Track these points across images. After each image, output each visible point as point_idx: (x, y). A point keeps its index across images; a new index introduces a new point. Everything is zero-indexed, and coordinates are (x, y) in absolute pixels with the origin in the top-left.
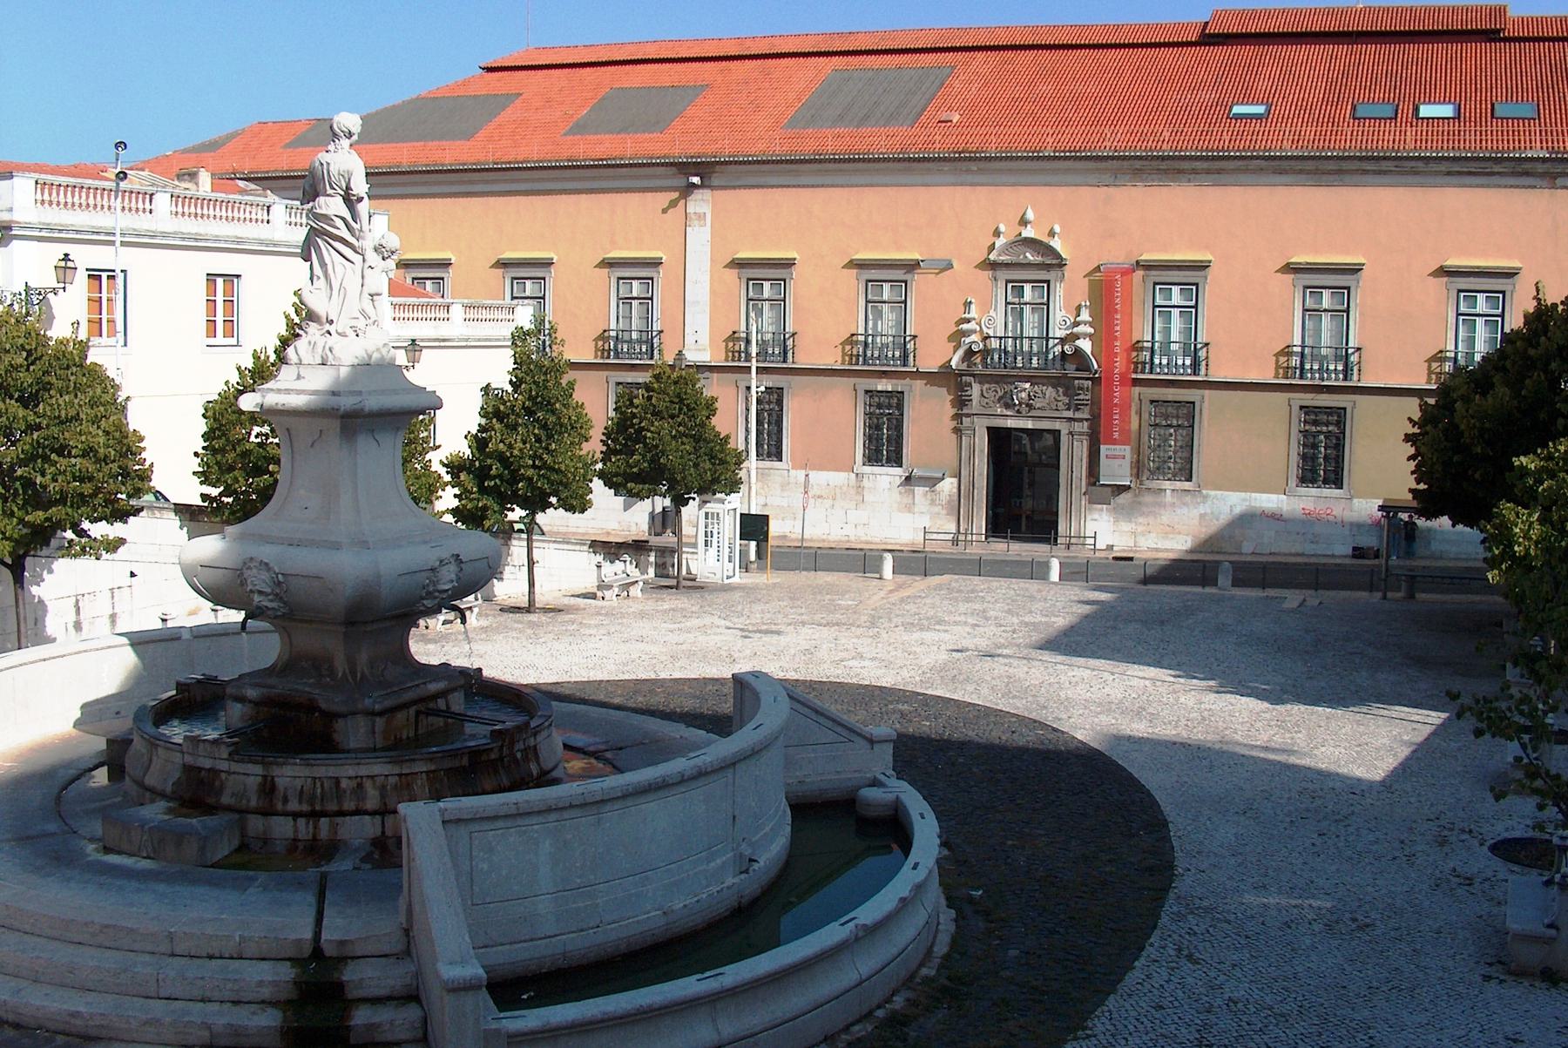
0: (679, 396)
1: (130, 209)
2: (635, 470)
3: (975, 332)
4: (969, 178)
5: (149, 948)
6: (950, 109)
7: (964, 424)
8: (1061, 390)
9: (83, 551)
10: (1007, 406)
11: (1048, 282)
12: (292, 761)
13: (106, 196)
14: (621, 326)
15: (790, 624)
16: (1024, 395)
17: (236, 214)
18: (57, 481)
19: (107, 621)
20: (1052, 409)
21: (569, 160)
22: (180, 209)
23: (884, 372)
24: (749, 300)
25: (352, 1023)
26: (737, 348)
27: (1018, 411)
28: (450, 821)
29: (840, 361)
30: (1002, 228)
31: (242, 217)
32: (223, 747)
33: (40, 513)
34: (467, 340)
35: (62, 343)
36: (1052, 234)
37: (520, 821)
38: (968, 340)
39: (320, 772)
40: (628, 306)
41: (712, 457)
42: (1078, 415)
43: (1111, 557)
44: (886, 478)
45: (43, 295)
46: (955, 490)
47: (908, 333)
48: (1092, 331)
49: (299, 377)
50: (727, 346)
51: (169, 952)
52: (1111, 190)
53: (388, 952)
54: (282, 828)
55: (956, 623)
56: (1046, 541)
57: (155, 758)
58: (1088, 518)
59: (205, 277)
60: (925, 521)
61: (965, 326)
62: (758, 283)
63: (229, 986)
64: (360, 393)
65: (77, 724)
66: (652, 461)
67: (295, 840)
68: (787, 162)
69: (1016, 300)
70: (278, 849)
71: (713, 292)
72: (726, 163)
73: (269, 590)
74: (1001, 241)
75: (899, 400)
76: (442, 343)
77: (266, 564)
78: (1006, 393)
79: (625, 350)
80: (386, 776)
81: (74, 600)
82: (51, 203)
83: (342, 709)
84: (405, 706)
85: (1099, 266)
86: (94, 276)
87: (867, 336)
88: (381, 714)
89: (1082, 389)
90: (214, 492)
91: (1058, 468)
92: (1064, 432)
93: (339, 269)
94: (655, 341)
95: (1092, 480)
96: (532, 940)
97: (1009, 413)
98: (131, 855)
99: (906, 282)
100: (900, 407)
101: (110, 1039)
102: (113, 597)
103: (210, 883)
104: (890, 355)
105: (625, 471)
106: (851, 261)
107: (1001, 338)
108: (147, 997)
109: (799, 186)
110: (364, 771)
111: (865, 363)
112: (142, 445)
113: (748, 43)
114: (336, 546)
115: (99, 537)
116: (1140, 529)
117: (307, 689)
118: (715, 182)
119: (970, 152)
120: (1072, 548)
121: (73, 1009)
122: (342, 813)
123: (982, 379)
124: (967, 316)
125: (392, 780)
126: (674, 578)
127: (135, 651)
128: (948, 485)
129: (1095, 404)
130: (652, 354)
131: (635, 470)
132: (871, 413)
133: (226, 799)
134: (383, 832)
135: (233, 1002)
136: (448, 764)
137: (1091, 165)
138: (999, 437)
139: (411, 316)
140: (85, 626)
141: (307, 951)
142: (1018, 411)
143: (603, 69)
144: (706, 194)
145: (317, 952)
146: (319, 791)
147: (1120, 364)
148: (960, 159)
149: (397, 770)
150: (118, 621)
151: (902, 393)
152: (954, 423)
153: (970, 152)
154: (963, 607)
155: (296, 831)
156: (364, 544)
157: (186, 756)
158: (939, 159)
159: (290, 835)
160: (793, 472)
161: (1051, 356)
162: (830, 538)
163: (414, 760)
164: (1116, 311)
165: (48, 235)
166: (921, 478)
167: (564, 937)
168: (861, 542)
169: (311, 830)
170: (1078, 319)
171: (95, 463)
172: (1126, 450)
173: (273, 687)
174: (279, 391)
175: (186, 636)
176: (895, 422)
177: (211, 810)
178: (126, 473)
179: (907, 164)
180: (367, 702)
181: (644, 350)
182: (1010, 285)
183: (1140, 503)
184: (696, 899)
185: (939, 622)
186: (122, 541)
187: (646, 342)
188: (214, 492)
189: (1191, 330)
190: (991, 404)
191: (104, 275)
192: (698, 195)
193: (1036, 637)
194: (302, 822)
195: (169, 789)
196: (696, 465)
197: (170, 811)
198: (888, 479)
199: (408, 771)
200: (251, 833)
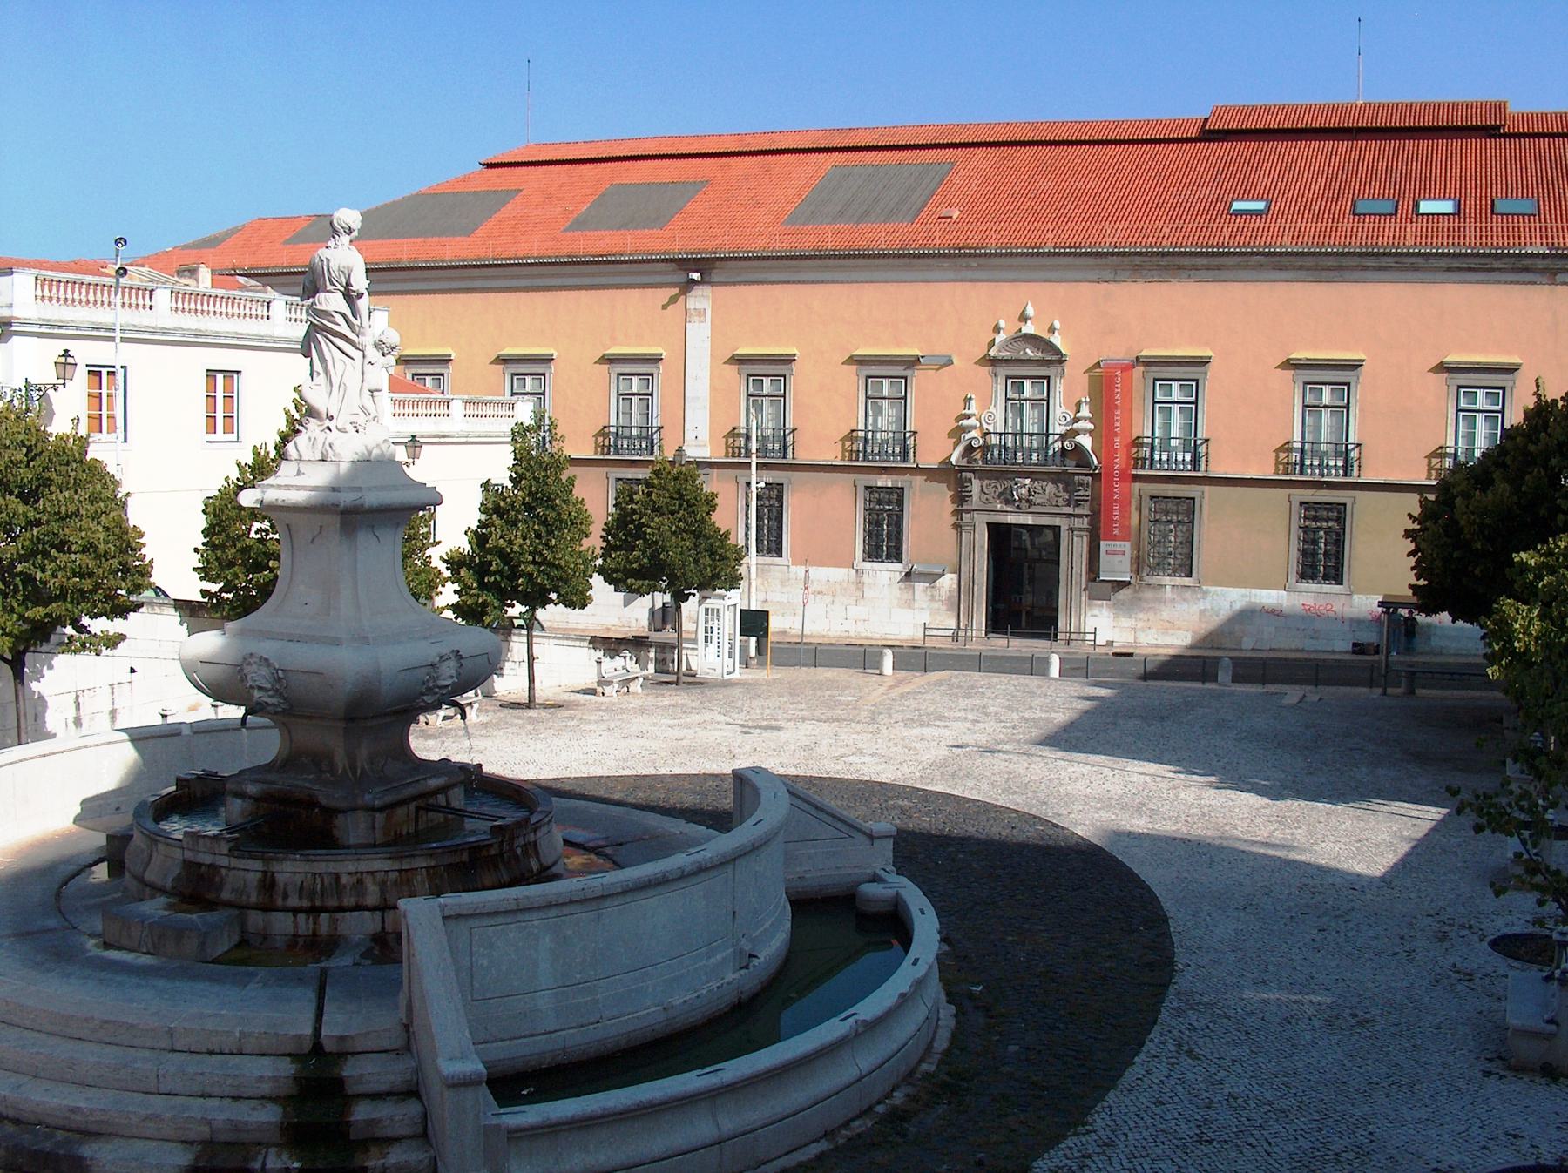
0: (679, 492)
1: (130, 305)
2: (635, 566)
3: (975, 428)
4: (969, 274)
6: (950, 205)
7: (964, 520)
8: (1061, 486)
9: (83, 647)
10: (1007, 502)
11: (1048, 378)
12: (292, 856)
13: (106, 292)
14: (621, 422)
15: (790, 720)
16: (1024, 491)
17: (236, 310)
19: (107, 717)
21: (569, 257)
22: (180, 305)
23: (884, 468)
24: (749, 396)
26: (737, 444)
27: (1018, 507)
28: (449, 917)
29: (840, 458)
30: (1002, 324)
31: (242, 313)
32: (223, 843)
36: (1052, 330)
37: (520, 917)
38: (968, 436)
39: (321, 867)
41: (712, 553)
42: (1078, 511)
44: (887, 573)
46: (955, 586)
47: (908, 429)
49: (299, 473)
50: (727, 442)
52: (1111, 286)
54: (282, 924)
55: (956, 719)
56: (1046, 637)
57: (155, 854)
58: (1088, 614)
60: (925, 617)
61: (965, 422)
62: (758, 379)
63: (229, 1081)
64: (360, 489)
65: (77, 820)
66: (652, 557)
67: (295, 936)
68: (787, 258)
69: (1016, 396)
70: (278, 945)
71: (713, 388)
72: (726, 259)
73: (269, 686)
74: (1000, 338)
75: (899, 496)
76: (442, 439)
77: (266, 660)
78: (1005, 489)
79: (625, 446)
81: (74, 695)
82: (51, 299)
83: (343, 805)
86: (94, 372)
87: (867, 432)
88: (381, 809)
89: (1082, 485)
90: (214, 588)
91: (1058, 564)
92: (1064, 528)
93: (339, 365)
94: (655, 436)
95: (1093, 576)
96: (532, 1035)
97: (1008, 509)
98: (131, 950)
99: (906, 378)
100: (900, 502)
102: (113, 693)
103: (213, 979)
105: (625, 566)
106: (851, 357)
107: (1001, 434)
108: (147, 1093)
109: (799, 282)
110: (363, 866)
111: (865, 459)
112: (142, 541)
114: (336, 642)
115: (99, 633)
118: (715, 278)
119: (970, 248)
120: (1072, 644)
121: (73, 1104)
122: (341, 909)
123: (982, 475)
124: (967, 411)
126: (674, 674)
127: (136, 747)
128: (948, 581)
129: (1095, 500)
130: (652, 450)
131: (635, 566)
132: (871, 509)
133: (226, 895)
134: (383, 928)
135: (233, 1098)
137: (1091, 261)
138: (999, 534)
139: (411, 412)
140: (85, 722)
141: (307, 1046)
142: (1018, 507)
145: (317, 1048)
146: (319, 886)
147: (1120, 461)
148: (960, 255)
149: (397, 866)
151: (902, 488)
152: (954, 520)
153: (970, 248)
154: (963, 703)
155: (296, 927)
156: (364, 640)
158: (940, 255)
159: (290, 930)
160: (793, 568)
161: (1051, 452)
162: (830, 634)
163: (413, 856)
165: (48, 331)
166: (920, 574)
167: (564, 1032)
168: (862, 638)
169: (311, 926)
170: (1078, 415)
171: (95, 559)
173: (273, 783)
174: (279, 487)
175: (186, 732)
176: (895, 518)
177: (211, 905)
178: (126, 569)
179: (907, 261)
181: (644, 446)
182: (1010, 381)
183: (1140, 599)
185: (940, 718)
187: (646, 438)
188: (214, 588)
189: (1191, 426)
190: (991, 500)
191: (104, 371)
192: (698, 291)
193: (1036, 733)
194: (302, 917)
195: (169, 884)
196: (696, 561)
197: (170, 907)
199: (405, 867)
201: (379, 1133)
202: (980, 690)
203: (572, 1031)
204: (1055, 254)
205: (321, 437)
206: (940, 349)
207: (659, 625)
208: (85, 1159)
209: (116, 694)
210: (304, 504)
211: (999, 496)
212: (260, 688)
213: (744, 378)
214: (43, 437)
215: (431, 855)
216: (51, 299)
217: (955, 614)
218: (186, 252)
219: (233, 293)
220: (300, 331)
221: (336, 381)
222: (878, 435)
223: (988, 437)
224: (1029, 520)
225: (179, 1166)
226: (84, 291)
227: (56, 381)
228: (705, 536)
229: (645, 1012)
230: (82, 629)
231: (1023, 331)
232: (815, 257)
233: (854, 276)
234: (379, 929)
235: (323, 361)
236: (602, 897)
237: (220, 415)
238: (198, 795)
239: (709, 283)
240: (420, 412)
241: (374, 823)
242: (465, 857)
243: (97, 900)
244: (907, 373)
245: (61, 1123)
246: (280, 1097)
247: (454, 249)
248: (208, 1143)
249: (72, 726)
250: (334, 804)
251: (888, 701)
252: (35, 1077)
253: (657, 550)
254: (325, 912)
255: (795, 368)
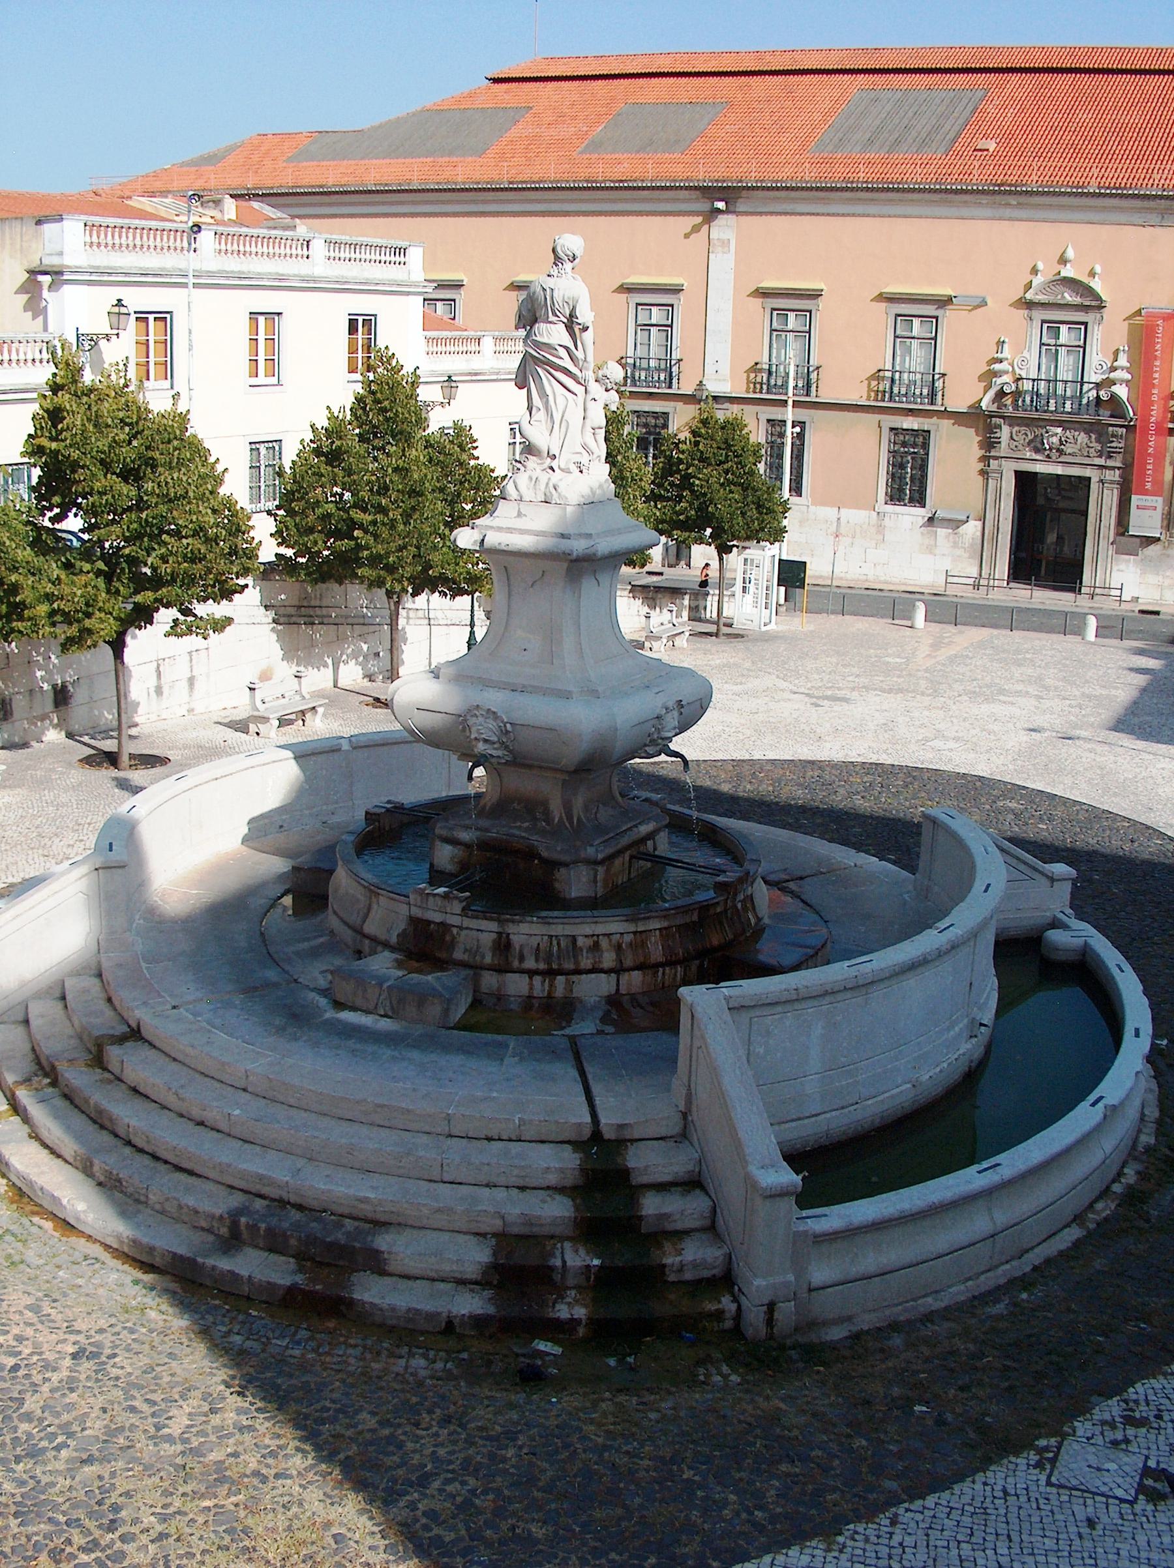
0: (726, 442)
1: (176, 249)
2: (681, 517)
3: (1007, 372)
4: (1008, 212)
5: (427, 1129)
6: (985, 136)
7: (992, 467)
8: (1093, 436)
9: (190, 631)
10: (1037, 450)
11: (1086, 324)
12: (529, 919)
13: (152, 236)
14: (639, 354)
15: (853, 689)
16: (1055, 440)
17: (277, 250)
18: (167, 562)
19: (184, 684)
20: (1082, 455)
21: (587, 181)
22: (223, 247)
23: (911, 410)
24: (772, 330)
25: (644, 1213)
26: (759, 379)
27: (1048, 456)
28: (734, 1008)
29: (865, 397)
30: (1040, 266)
31: (283, 253)
32: (456, 903)
33: (150, 593)
34: (497, 374)
35: (163, 416)
36: (1092, 274)
37: (797, 1006)
38: (999, 381)
39: (558, 930)
40: (647, 333)
41: (759, 506)
42: (1110, 463)
43: (1137, 609)
44: (910, 517)
45: (94, 340)
46: (979, 534)
47: (937, 371)
48: (1129, 377)
49: (520, 514)
50: (748, 377)
51: (446, 1132)
52: (1158, 230)
53: (663, 1135)
54: (517, 985)
55: (1019, 693)
56: (1072, 590)
57: (375, 906)
58: (1115, 568)
59: (248, 316)
60: (946, 564)
61: (997, 367)
62: (783, 313)
63: (516, 1172)
64: (589, 536)
65: (246, 840)
66: (699, 509)
67: (530, 997)
68: (817, 189)
69: (1052, 342)
70: (512, 1006)
71: (736, 322)
72: (753, 188)
73: (495, 739)
74: (1038, 281)
75: (924, 438)
76: (475, 377)
77: (494, 713)
78: (1036, 436)
79: (643, 378)
80: (622, 934)
81: (155, 664)
82: (99, 245)
83: (566, 858)
84: (620, 852)
85: (1140, 310)
86: (142, 317)
87: (894, 372)
88: (602, 862)
89: (1113, 436)
90: (289, 552)
91: (1085, 514)
92: (1094, 480)
93: (561, 402)
94: (673, 369)
95: (1122, 530)
96: (799, 1119)
97: (1038, 457)
98: (367, 1012)
99: (937, 318)
100: (926, 446)
101: (399, 1224)
102: (191, 660)
103: (464, 1050)
104: (918, 392)
105: (671, 518)
106: (881, 294)
107: (1034, 380)
108: (430, 1181)
109: (828, 215)
110: (600, 929)
111: (891, 400)
112: (250, 523)
113: (768, 58)
114: (566, 695)
115: (205, 616)
116: (1167, 582)
117: (523, 834)
118: (741, 207)
119: (1010, 185)
120: (1096, 598)
121: (362, 1194)
122: (578, 972)
123: (1012, 421)
124: (999, 355)
125: (628, 938)
126: (713, 623)
127: (300, 766)
128: (972, 528)
129: (1128, 452)
130: (671, 382)
131: (681, 517)
132: (895, 451)
133: (458, 955)
134: (618, 990)
135: (518, 1188)
136: (679, 921)
137: (1138, 203)
138: (1025, 481)
139: (444, 349)
140: (165, 690)
141: (587, 1133)
142: (1048, 456)
143: (616, 82)
144: (730, 219)
145: (596, 1134)
146: (555, 948)
147: (1155, 414)
148: (1000, 192)
149: (632, 928)
150: (197, 685)
151: (929, 432)
152: (981, 466)
153: (1010, 185)
154: (1017, 672)
155: (531, 988)
156: (595, 693)
157: (413, 908)
158: (978, 192)
159: (525, 991)
160: (812, 508)
161: (1085, 401)
162: (849, 576)
163: (649, 918)
164: (1155, 358)
165: (99, 278)
166: (943, 520)
167: (828, 1115)
168: (880, 582)
169: (547, 988)
170: (1115, 364)
171: (205, 542)
172: (1158, 502)
173: (487, 830)
174: (500, 529)
175: (346, 746)
176: (920, 462)
177: (441, 965)
178: (234, 551)
179: (943, 196)
180: (590, 851)
181: (662, 378)
182: (1045, 326)
183: (1168, 556)
184: (938, 1069)
185: (1002, 691)
186: (229, 621)
187: (665, 370)
188: (289, 552)
190: (1020, 447)
191: (151, 317)
192: (722, 220)
193: (1108, 714)
194: (537, 980)
195: (394, 940)
196: (743, 514)
197: (399, 965)
198: (910, 518)
199: (642, 929)
200: (484, 989)
201: (670, 1227)
202: (1028, 656)
203: (834, 1113)
204: (1100, 194)
205: (544, 477)
206: (974, 290)
207: (673, 560)
208: (383, 1252)
209: (194, 661)
210: (532, 550)
211: (1029, 444)
212: (486, 741)
213: (768, 312)
214: (142, 412)
215: (665, 917)
216: (99, 245)
217: (978, 562)
218: (185, 169)
219: (274, 233)
220: (514, 362)
221: (557, 417)
222: (905, 376)
223: (1020, 383)
224: (1059, 470)
225: (479, 1262)
226: (130, 235)
227: (109, 331)
228: (753, 489)
229: (898, 1090)
230: (186, 612)
231: (1063, 274)
232: (847, 189)
233: (886, 209)
234: (613, 991)
235: (543, 395)
236: (872, 982)
237: (261, 358)
238: (387, 828)
239: (734, 212)
240: (452, 349)
241: (595, 877)
242: (695, 918)
243: (306, 945)
244: (939, 313)
245: (346, 1211)
246: (565, 1187)
247: (466, 171)
248: (502, 1237)
249: (153, 694)
250: (555, 856)
251: (939, 667)
252: (310, 1159)
253: (705, 502)
254: (562, 974)
255: (821, 302)
